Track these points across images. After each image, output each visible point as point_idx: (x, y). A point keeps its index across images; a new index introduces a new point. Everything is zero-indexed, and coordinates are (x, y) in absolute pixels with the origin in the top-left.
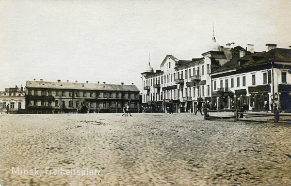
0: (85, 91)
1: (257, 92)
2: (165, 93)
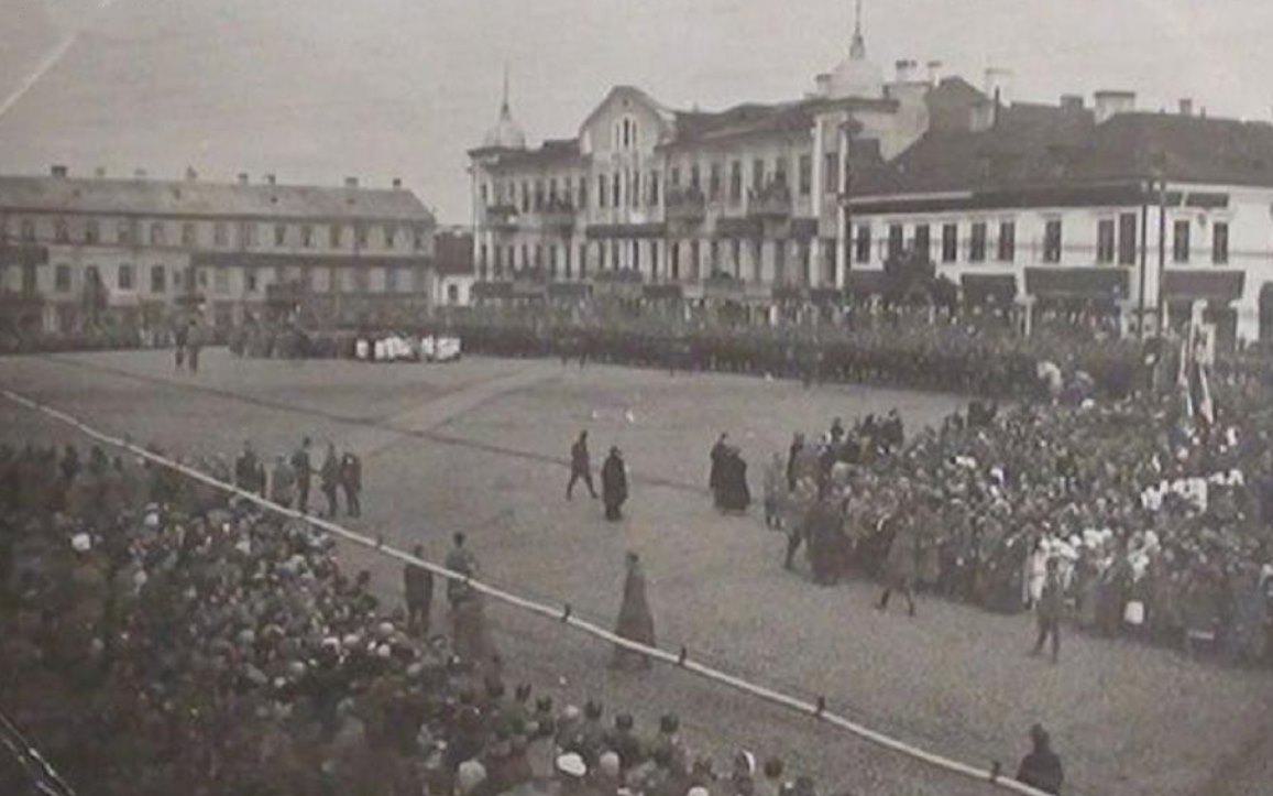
0: (189, 219)
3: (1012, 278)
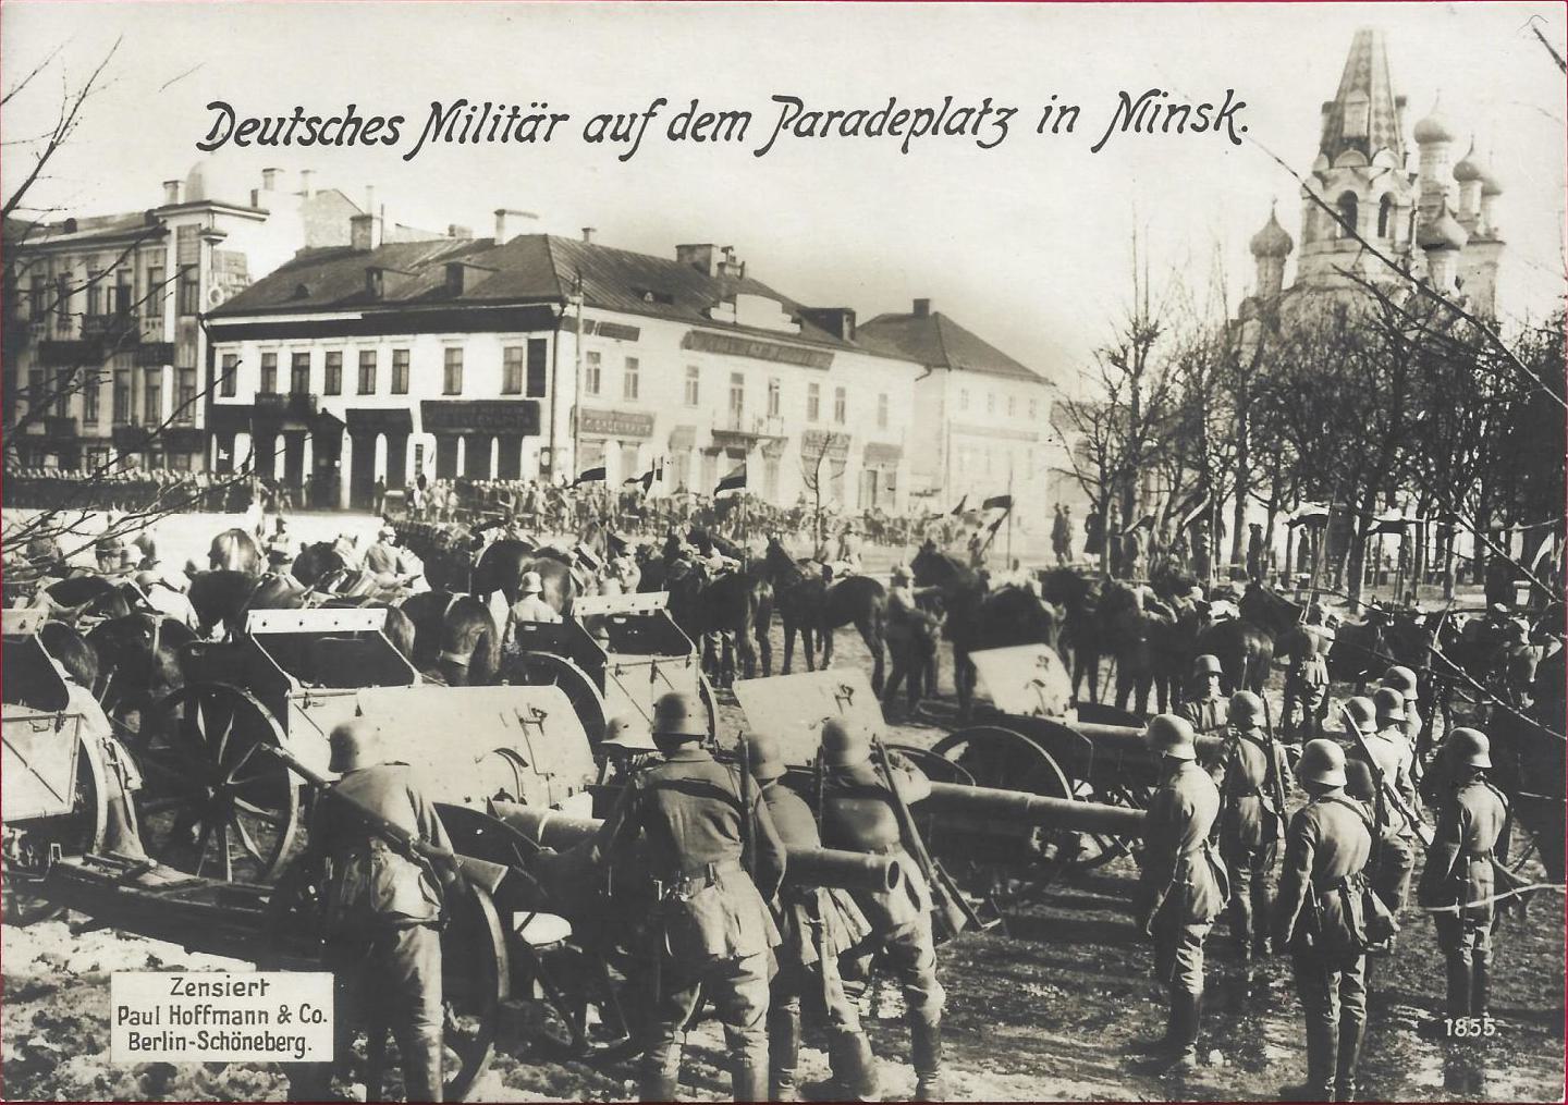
3: (406, 413)
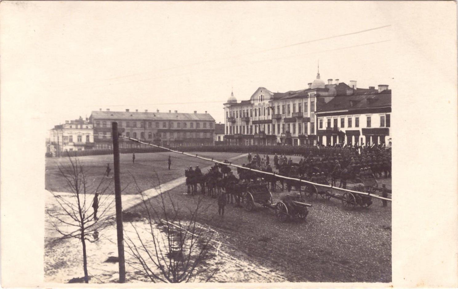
1: (373, 135)
2: (256, 127)
